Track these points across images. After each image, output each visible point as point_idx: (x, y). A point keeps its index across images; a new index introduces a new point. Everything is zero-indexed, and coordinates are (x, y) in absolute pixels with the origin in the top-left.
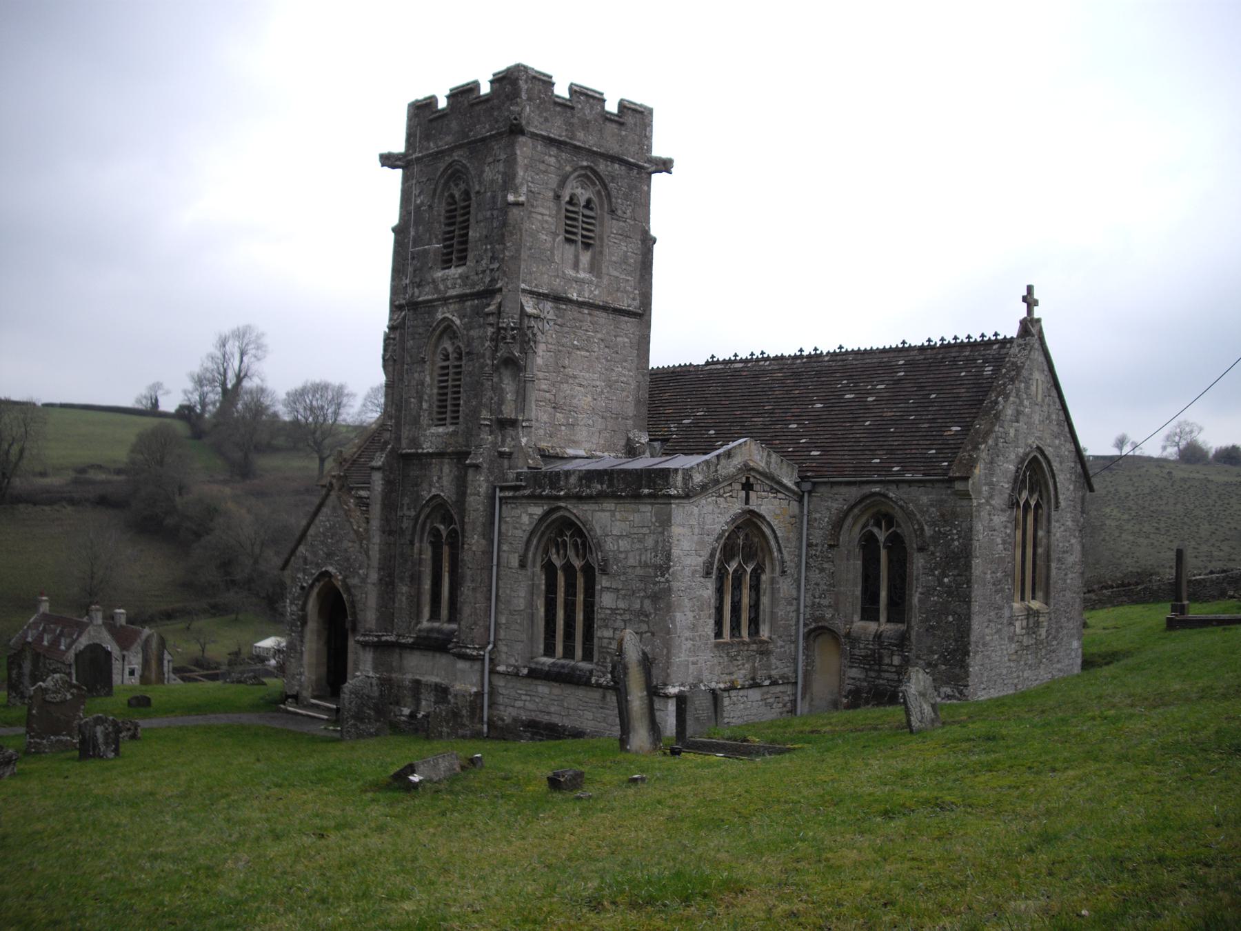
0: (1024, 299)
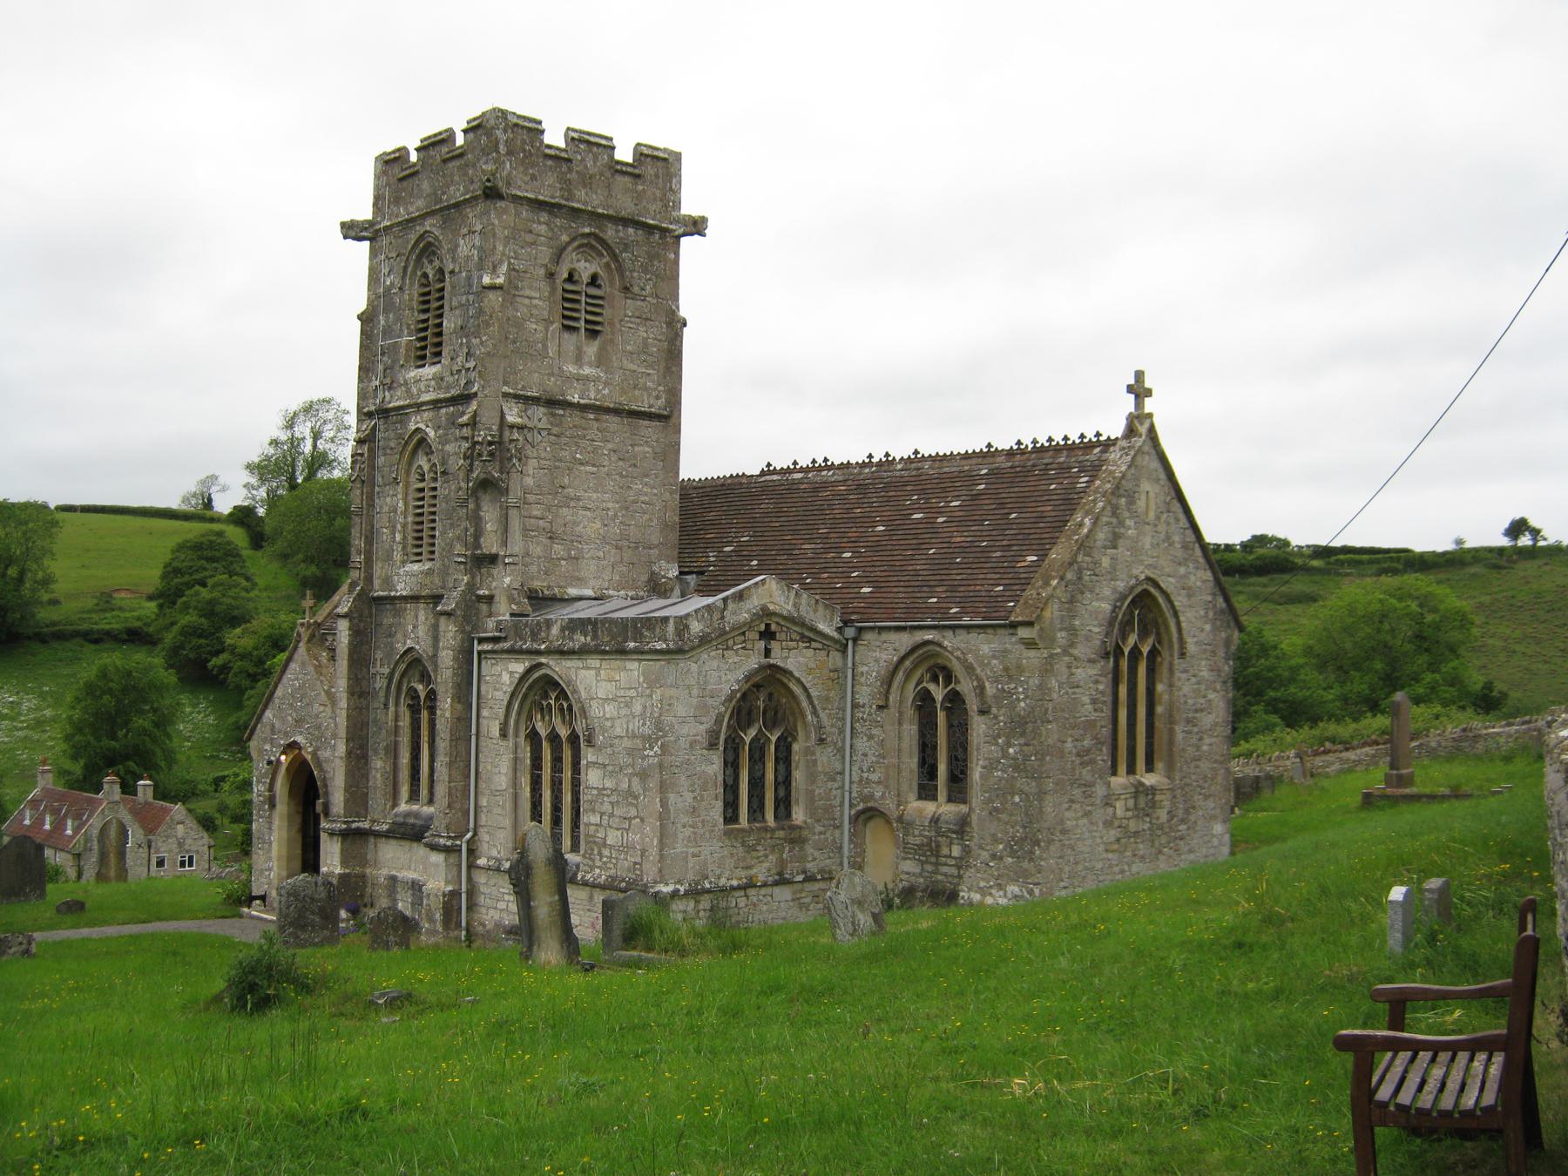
0: (1130, 389)
